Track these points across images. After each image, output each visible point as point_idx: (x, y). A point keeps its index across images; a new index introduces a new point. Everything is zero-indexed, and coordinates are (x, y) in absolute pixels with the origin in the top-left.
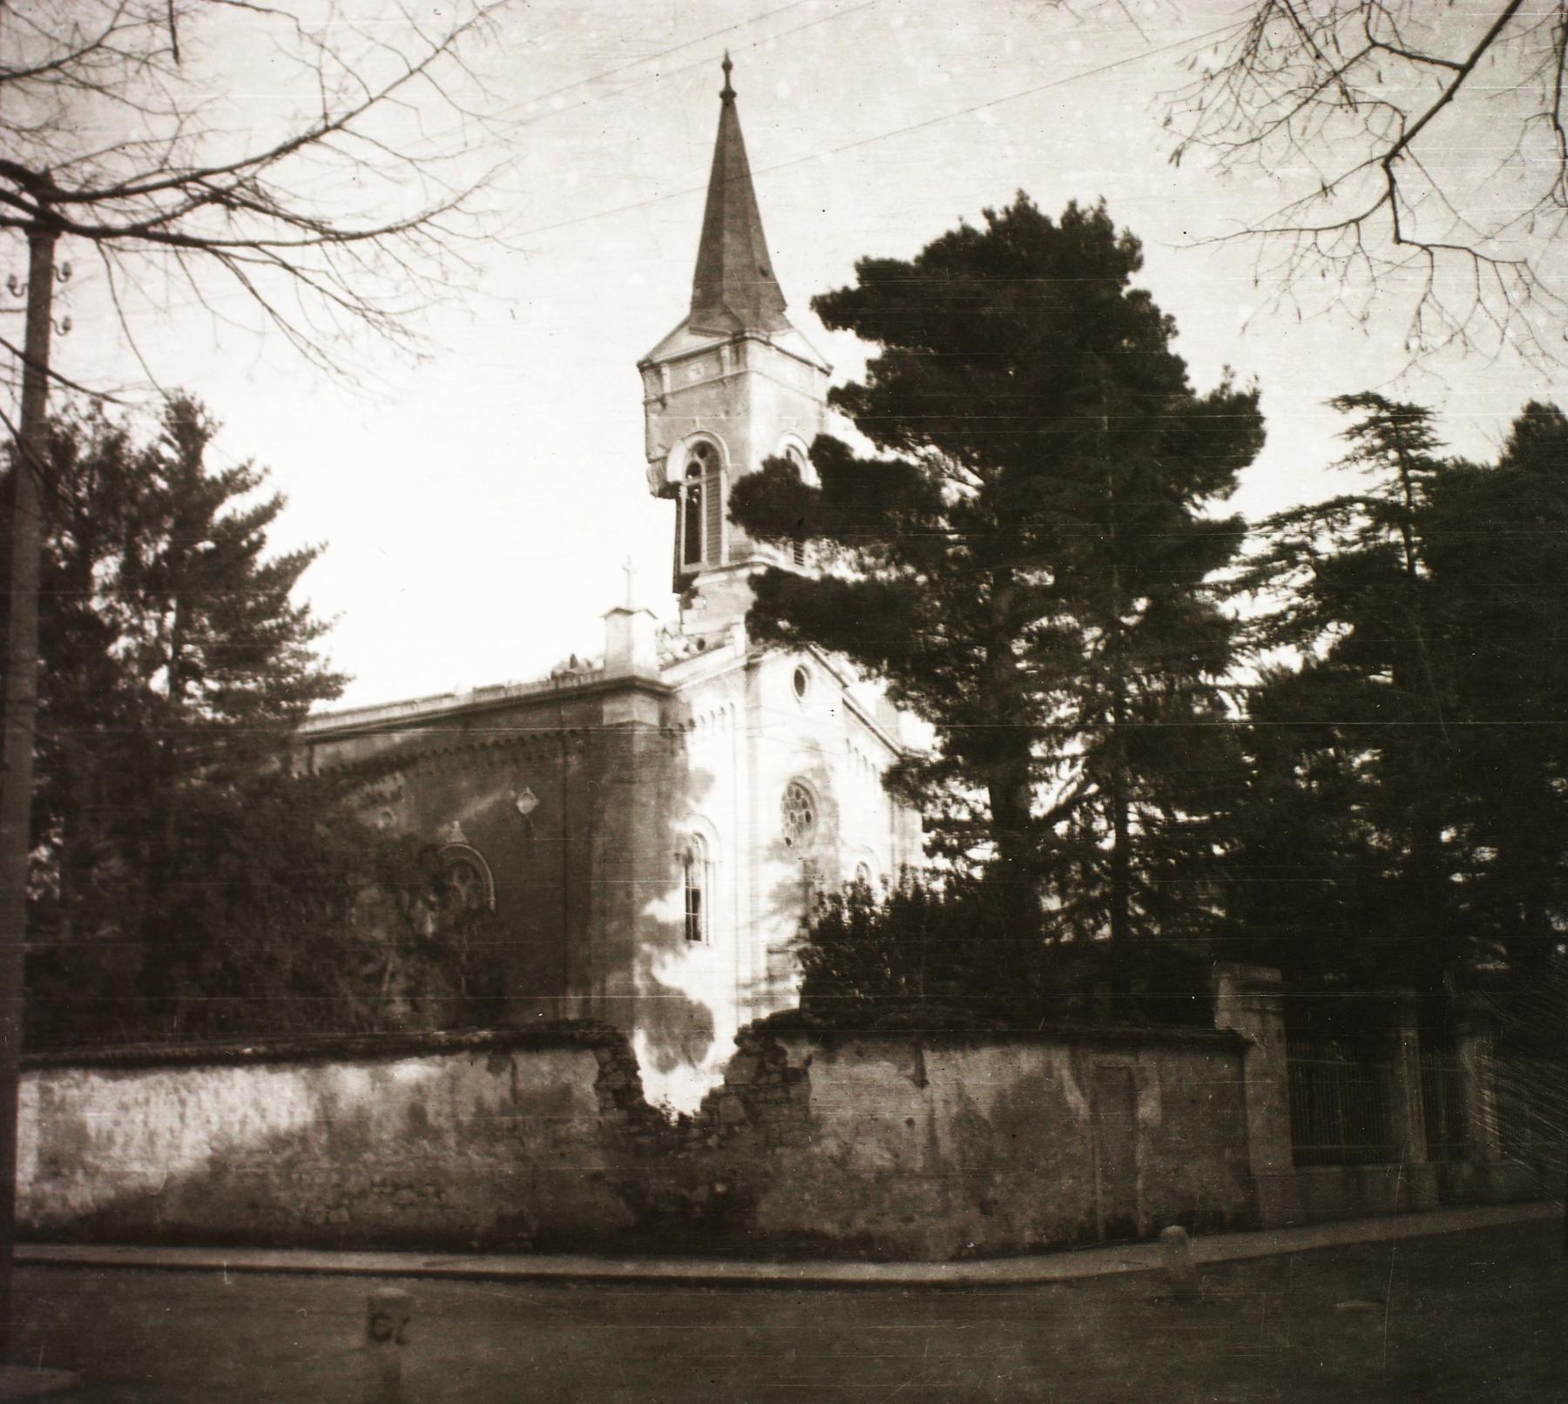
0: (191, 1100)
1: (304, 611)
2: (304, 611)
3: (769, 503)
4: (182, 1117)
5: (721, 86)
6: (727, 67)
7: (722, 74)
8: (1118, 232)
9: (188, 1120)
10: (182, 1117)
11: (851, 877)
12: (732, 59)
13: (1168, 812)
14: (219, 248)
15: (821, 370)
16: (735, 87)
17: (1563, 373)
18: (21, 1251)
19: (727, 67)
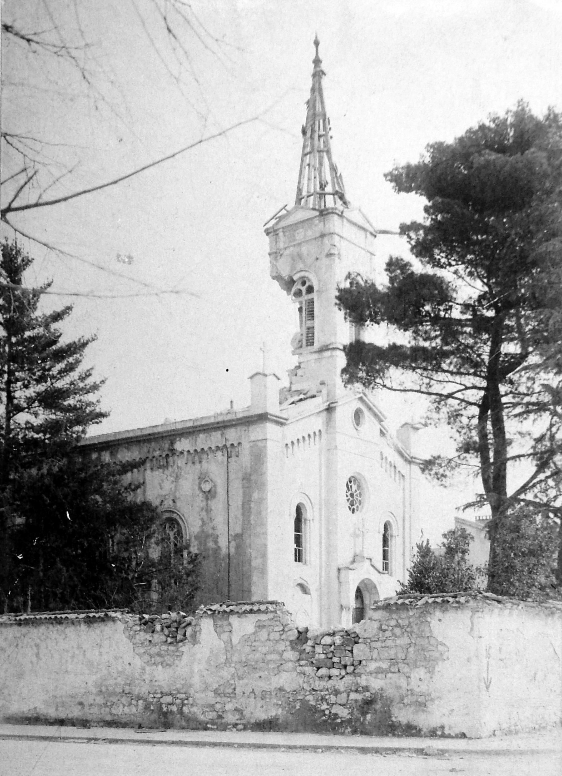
0: (43, 645)
1: (76, 348)
2: (76, 348)
3: (358, 303)
4: (37, 655)
5: (313, 57)
6: (317, 43)
7: (314, 47)
8: (487, 123)
9: (41, 656)
10: (37, 655)
11: (219, 534)
12: (319, 38)
13: (42, 571)
14: (535, 481)
15: (371, 233)
16: (321, 56)
17: (558, 316)
18: (505, 406)
19: (317, 43)
